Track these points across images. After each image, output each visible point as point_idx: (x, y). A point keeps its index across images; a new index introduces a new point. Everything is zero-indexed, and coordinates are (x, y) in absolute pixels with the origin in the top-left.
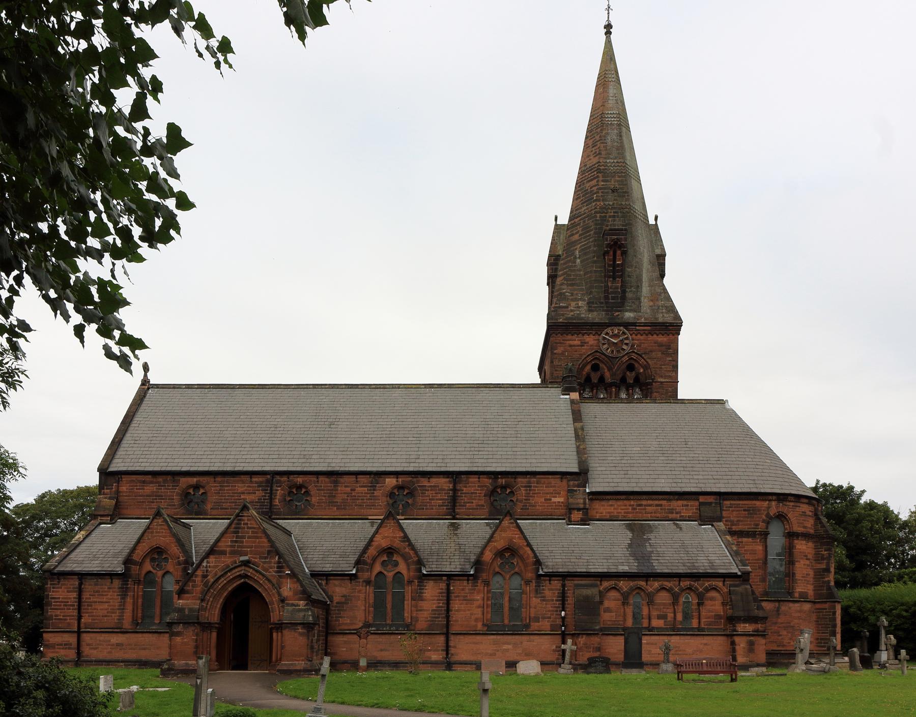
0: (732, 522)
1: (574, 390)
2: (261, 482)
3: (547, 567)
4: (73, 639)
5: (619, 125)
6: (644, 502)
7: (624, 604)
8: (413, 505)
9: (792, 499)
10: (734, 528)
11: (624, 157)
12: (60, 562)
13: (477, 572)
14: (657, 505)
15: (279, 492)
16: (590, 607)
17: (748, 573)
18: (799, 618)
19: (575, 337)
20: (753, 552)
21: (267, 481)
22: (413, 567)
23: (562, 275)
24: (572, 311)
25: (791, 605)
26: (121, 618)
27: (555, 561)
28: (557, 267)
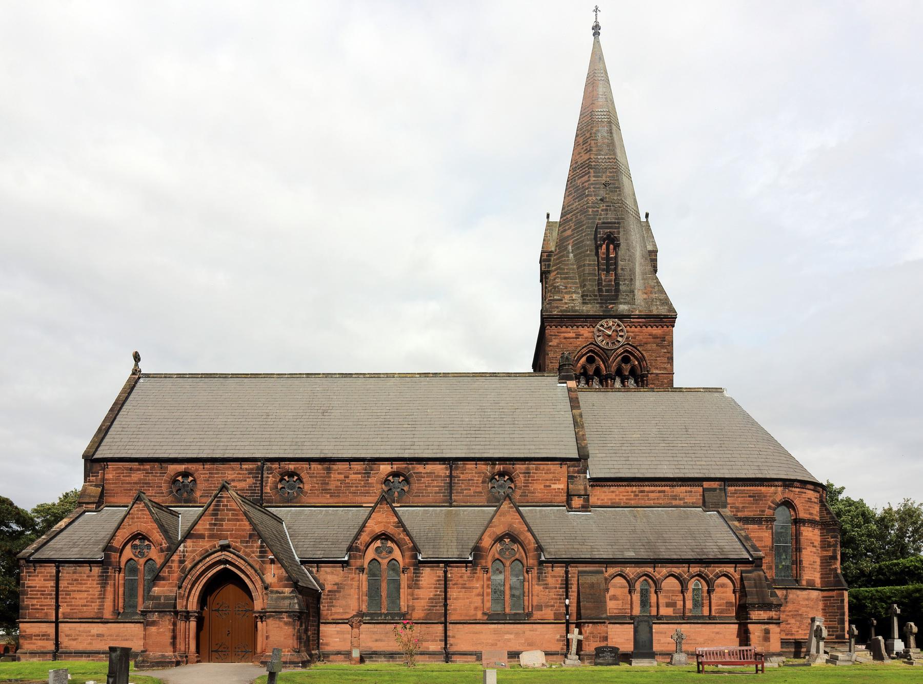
0: (737, 508)
1: (570, 379)
2: (252, 469)
3: (549, 553)
4: (50, 629)
5: (610, 122)
6: (646, 489)
7: (630, 592)
8: (408, 492)
9: (798, 484)
10: (740, 515)
11: (615, 154)
12: (37, 550)
13: (476, 558)
14: (659, 492)
15: (270, 480)
16: (597, 596)
17: (761, 559)
18: (807, 606)
21: (258, 468)
22: (408, 554)
23: (556, 270)
24: (566, 303)
25: (799, 592)
26: (101, 607)
27: (556, 547)
28: (549, 266)
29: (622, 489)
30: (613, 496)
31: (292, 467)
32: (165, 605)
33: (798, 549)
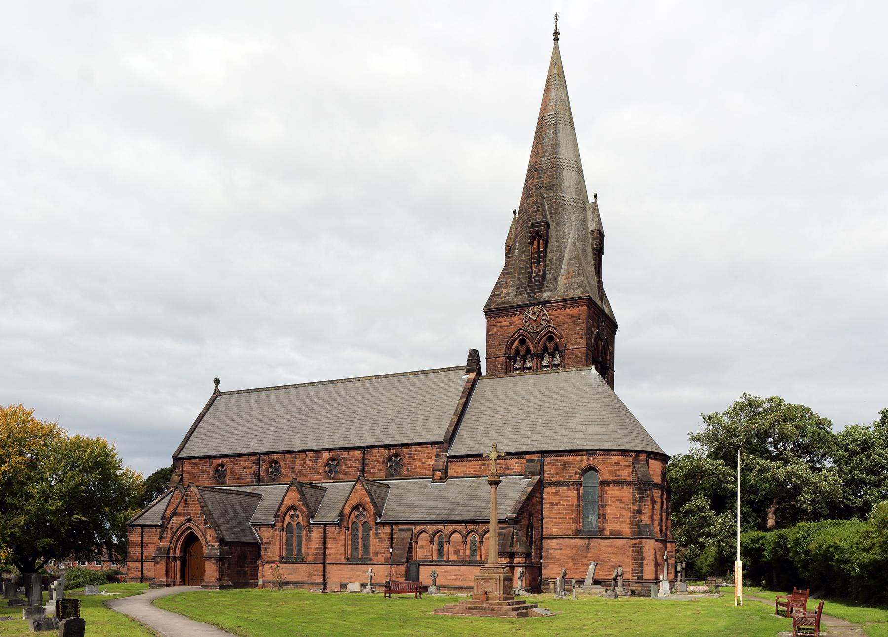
0: (552, 474)
4: (138, 565)
12: (135, 519)
15: (264, 466)
18: (609, 552)
19: (504, 319)
20: (568, 499)
25: (600, 541)
29: (471, 463)
30: (464, 469)
31: (275, 457)
32: (163, 553)
33: (603, 506)
